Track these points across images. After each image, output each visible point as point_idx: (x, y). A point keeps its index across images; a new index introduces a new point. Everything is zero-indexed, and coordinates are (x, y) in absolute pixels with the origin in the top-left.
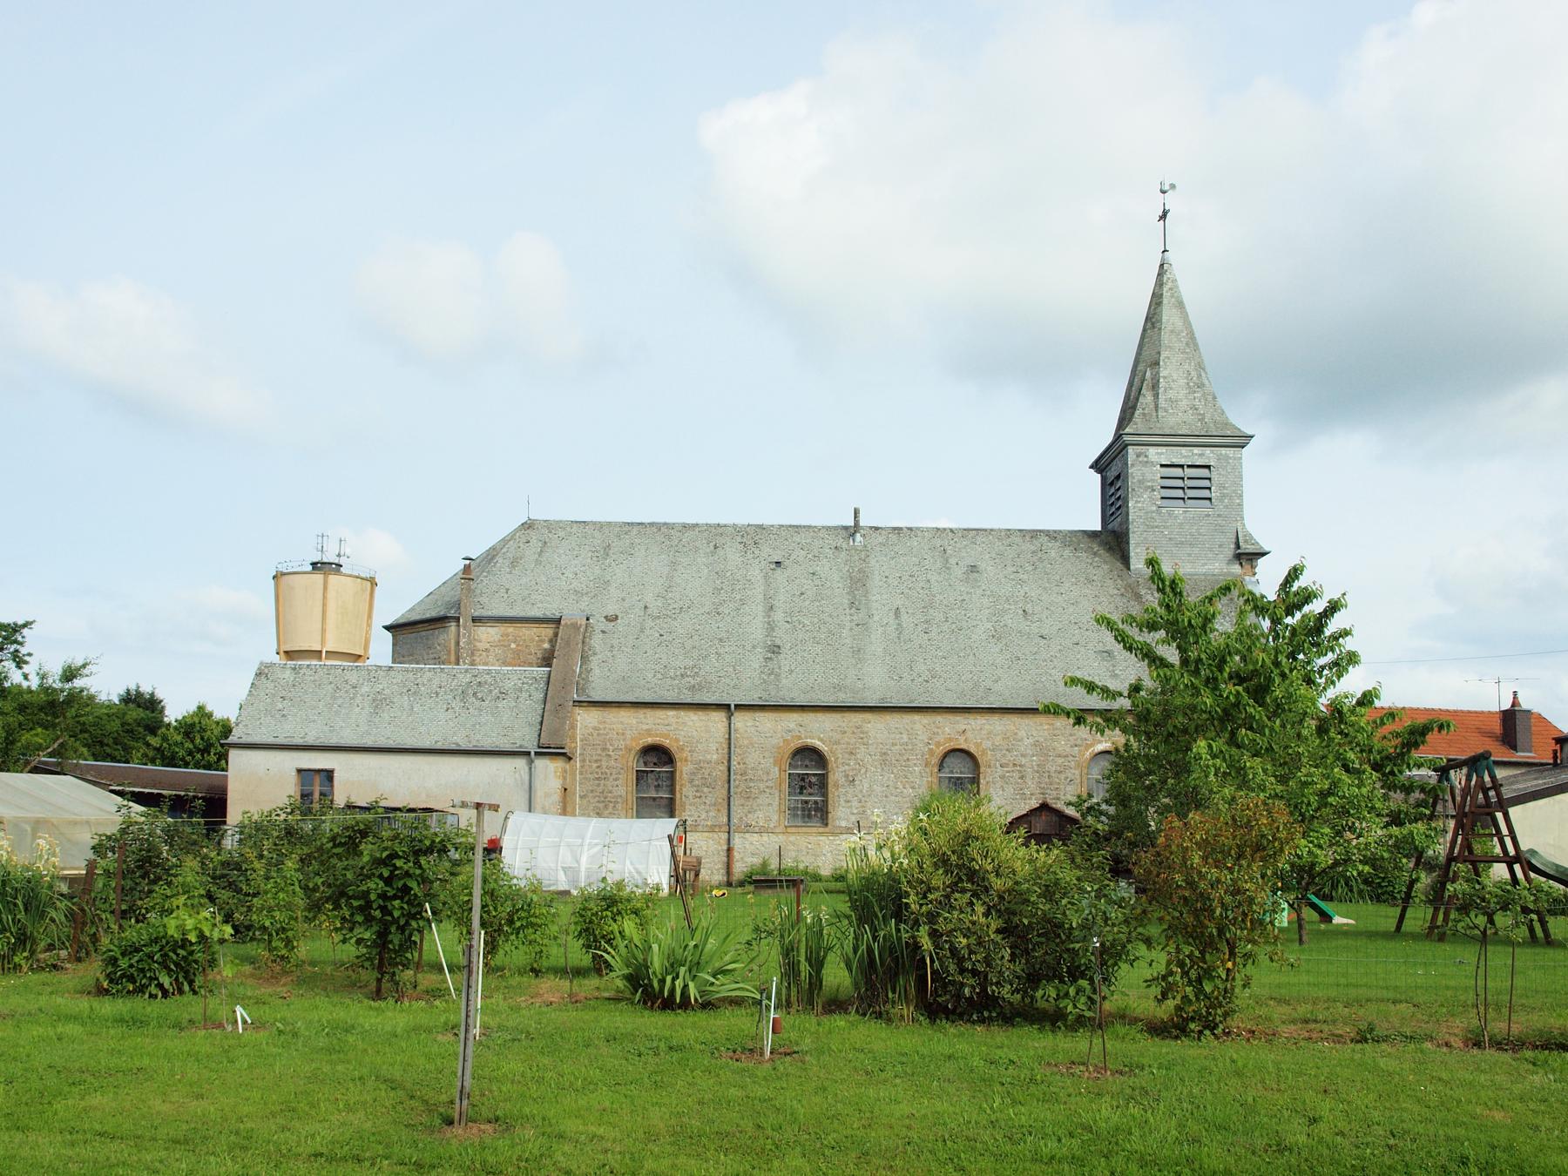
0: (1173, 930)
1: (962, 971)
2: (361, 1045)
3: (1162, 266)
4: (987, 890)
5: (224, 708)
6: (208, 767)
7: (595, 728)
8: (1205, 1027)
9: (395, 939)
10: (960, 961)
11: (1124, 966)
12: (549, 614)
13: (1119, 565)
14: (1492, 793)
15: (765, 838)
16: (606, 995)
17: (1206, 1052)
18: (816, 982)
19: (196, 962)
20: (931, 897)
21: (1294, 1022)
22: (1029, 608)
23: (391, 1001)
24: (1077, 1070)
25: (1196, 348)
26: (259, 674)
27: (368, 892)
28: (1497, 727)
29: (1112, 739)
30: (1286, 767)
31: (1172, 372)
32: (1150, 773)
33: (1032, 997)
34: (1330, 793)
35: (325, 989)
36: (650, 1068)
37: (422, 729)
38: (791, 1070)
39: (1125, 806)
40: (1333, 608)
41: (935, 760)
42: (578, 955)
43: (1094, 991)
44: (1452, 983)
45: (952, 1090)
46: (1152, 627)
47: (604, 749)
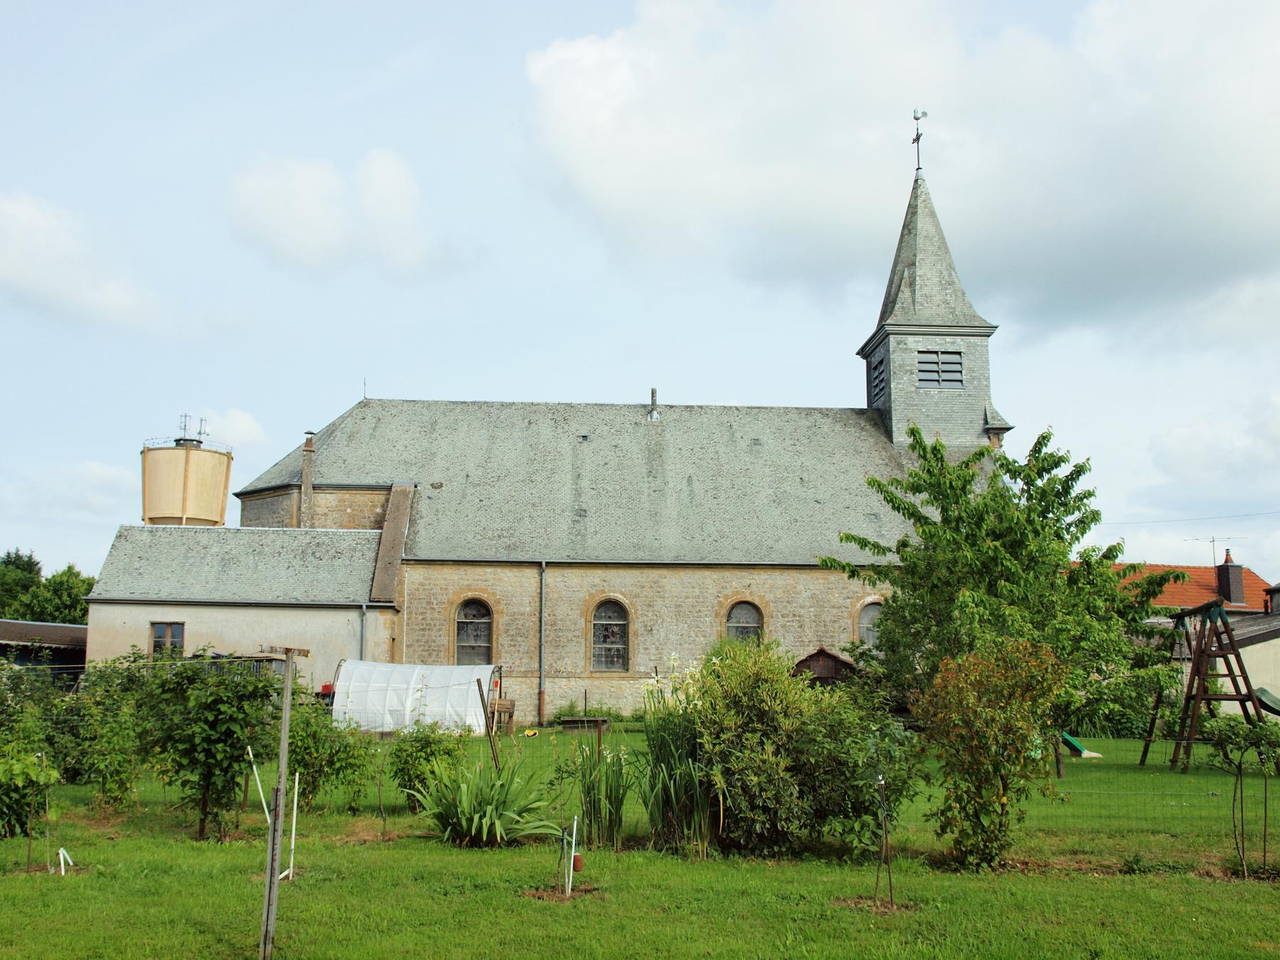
0: (950, 768)
1: (753, 808)
2: (176, 886)
3: (916, 181)
4: (776, 730)
5: (89, 568)
6: (73, 621)
7: (421, 584)
8: (982, 860)
9: (219, 781)
10: (752, 798)
11: (905, 801)
12: (381, 482)
13: (884, 439)
14: (1224, 637)
15: (573, 682)
16: (418, 833)
17: (985, 885)
18: (616, 820)
19: (28, 805)
20: (723, 737)
21: (1063, 853)
22: (805, 476)
23: (212, 841)
24: (866, 904)
25: (947, 251)
26: (119, 537)
27: (193, 735)
28: (1213, 581)
29: (885, 590)
30: (1042, 613)
31: (926, 271)
32: (915, 621)
33: (819, 832)
34: (1081, 638)
35: (151, 829)
36: (454, 907)
37: (265, 586)
38: (592, 909)
39: (894, 651)
40: (1079, 471)
41: (724, 612)
42: (394, 793)
43: (879, 826)
44: (1204, 813)
45: (746, 927)
46: (916, 489)
47: (429, 603)
